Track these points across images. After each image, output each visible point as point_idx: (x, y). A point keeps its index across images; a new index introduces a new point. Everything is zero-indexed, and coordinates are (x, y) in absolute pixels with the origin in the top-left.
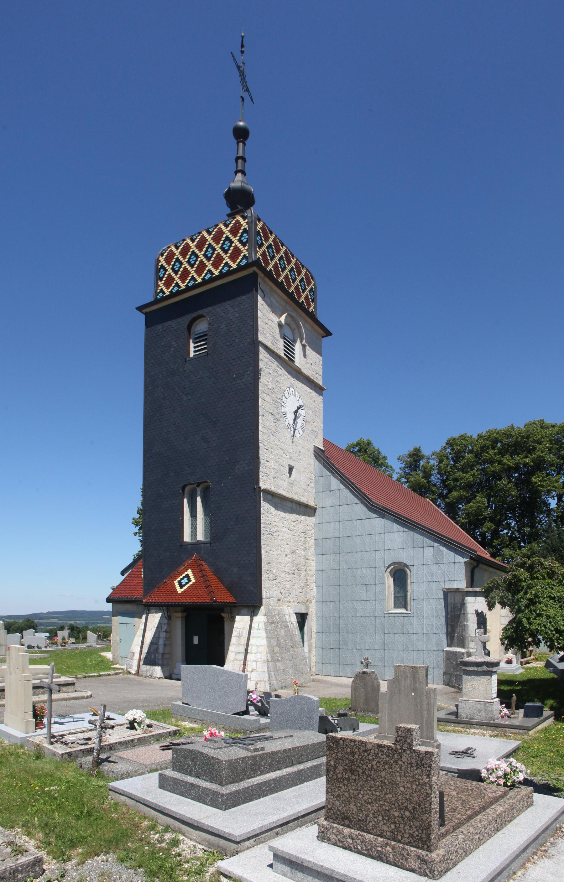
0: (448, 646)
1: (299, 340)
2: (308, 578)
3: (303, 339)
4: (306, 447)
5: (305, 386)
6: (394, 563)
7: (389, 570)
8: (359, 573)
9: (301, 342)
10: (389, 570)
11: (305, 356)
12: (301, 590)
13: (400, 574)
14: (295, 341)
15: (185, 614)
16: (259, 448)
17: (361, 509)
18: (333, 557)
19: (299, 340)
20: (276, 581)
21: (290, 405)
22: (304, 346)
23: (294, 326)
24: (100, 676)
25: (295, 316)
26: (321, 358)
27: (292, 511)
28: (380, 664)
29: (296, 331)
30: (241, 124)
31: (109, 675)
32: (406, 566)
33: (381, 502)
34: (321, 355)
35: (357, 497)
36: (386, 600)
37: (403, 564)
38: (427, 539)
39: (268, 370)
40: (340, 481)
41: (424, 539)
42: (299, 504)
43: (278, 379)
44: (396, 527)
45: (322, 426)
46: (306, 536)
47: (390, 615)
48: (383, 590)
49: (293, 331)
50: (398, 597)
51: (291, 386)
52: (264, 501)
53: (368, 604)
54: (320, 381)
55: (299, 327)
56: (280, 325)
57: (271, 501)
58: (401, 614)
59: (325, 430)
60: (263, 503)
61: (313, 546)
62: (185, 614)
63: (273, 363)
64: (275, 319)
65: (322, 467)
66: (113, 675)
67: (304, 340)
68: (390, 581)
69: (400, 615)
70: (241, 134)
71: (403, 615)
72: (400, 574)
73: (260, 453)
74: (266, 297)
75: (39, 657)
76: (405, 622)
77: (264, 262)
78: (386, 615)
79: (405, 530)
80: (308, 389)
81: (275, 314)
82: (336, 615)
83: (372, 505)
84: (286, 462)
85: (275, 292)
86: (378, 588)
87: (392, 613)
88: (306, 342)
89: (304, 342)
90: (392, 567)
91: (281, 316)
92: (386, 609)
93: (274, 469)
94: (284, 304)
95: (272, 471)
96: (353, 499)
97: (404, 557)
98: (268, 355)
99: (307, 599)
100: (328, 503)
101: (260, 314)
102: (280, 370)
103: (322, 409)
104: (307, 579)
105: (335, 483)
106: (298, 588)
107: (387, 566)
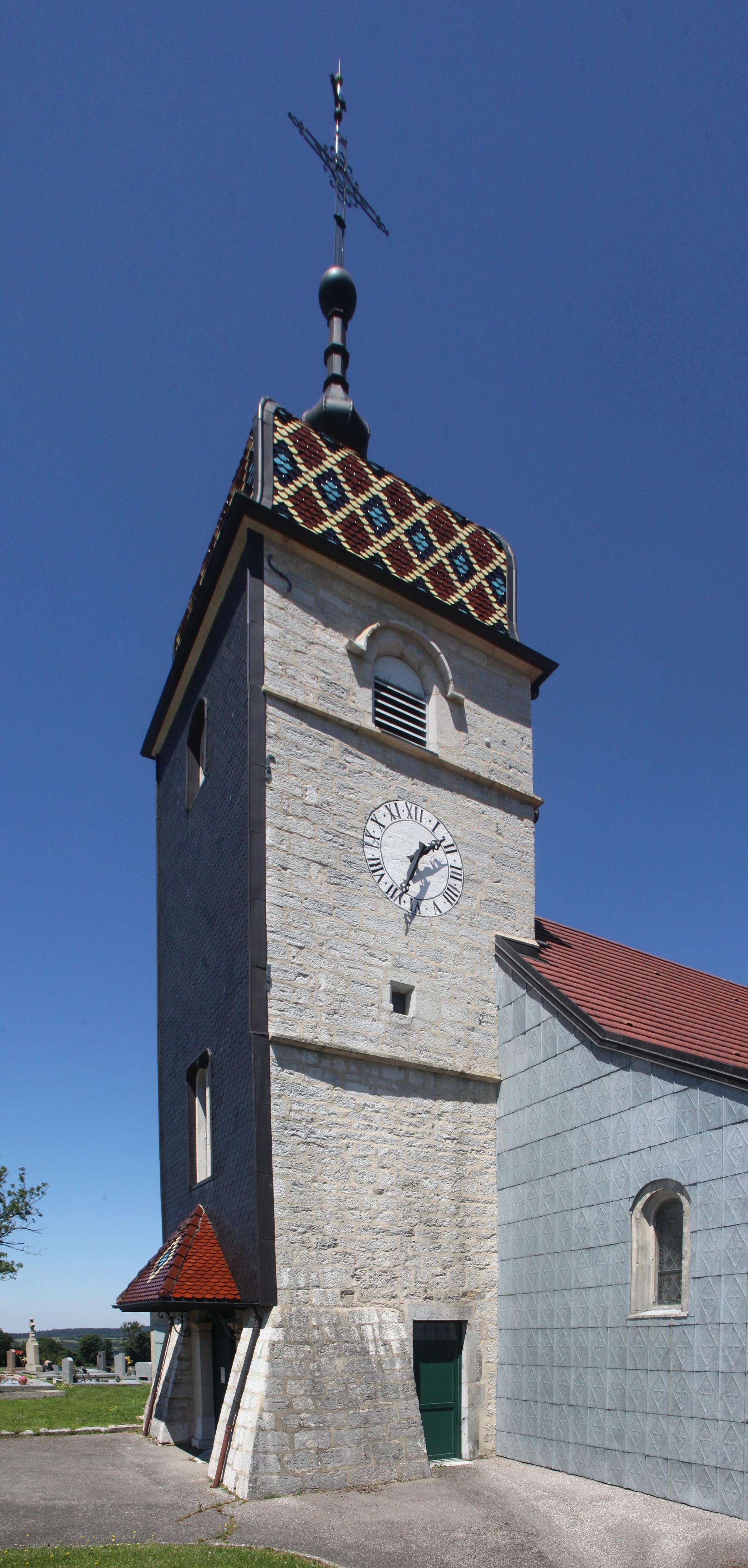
0: (207, 1459)
1: (435, 689)
2: (469, 1242)
3: (448, 683)
4: (463, 941)
5: (459, 797)
6: (653, 1184)
7: (640, 1205)
8: (575, 1220)
9: (444, 692)
10: (640, 1205)
11: (461, 724)
12: (439, 1270)
13: (665, 1211)
14: (427, 695)
15: (209, 1326)
16: (264, 944)
17: (582, 1059)
18: (527, 1188)
19: (435, 689)
20: (337, 1249)
21: (396, 845)
22: (455, 704)
23: (416, 656)
24: (73, 1433)
25: (411, 628)
26: (528, 731)
27: (405, 1090)
28: (615, 1446)
29: (427, 670)
30: (334, 272)
31: (99, 1432)
32: (680, 1187)
33: (617, 1022)
34: (526, 722)
35: (573, 1030)
36: (633, 1284)
37: (672, 1185)
38: (730, 1102)
39: (302, 761)
40: (542, 1001)
41: (723, 1102)
42: (463, 1078)
43: (349, 782)
44: (657, 1085)
45: (532, 890)
46: (458, 1147)
47: (639, 1323)
48: (625, 1260)
49: (417, 670)
50: (669, 1273)
51: (400, 798)
52: (283, 1065)
53: (592, 1296)
54: (525, 786)
55: (433, 658)
56: (355, 655)
57: (316, 1066)
58: (665, 1318)
59: (539, 900)
60: (274, 1069)
61: (493, 1170)
62: (209, 1326)
63: (323, 743)
64: (339, 642)
65: (510, 979)
66: (106, 1432)
67: (452, 685)
68: (646, 1234)
69: (662, 1323)
70: (338, 298)
71: (668, 1322)
72: (665, 1211)
73: (270, 954)
74: (294, 591)
75: (43, 1396)
76: (675, 1340)
77: (300, 515)
78: (629, 1323)
79: (677, 1087)
80: (473, 804)
81: (337, 629)
82: (533, 1325)
83: (602, 1042)
84: (382, 978)
85: (335, 576)
86: (611, 1256)
87: (643, 1319)
88: (456, 688)
89: (451, 691)
90: (648, 1195)
91: (359, 633)
92: (633, 1309)
93: (328, 992)
94: (374, 604)
95: (323, 996)
96: (564, 1037)
97: (670, 1165)
98: (304, 725)
99: (462, 1290)
100: (521, 1063)
101: (269, 629)
102: (357, 760)
103: (532, 850)
104: (463, 1245)
105: (535, 1010)
106: (428, 1265)
107: (635, 1194)
